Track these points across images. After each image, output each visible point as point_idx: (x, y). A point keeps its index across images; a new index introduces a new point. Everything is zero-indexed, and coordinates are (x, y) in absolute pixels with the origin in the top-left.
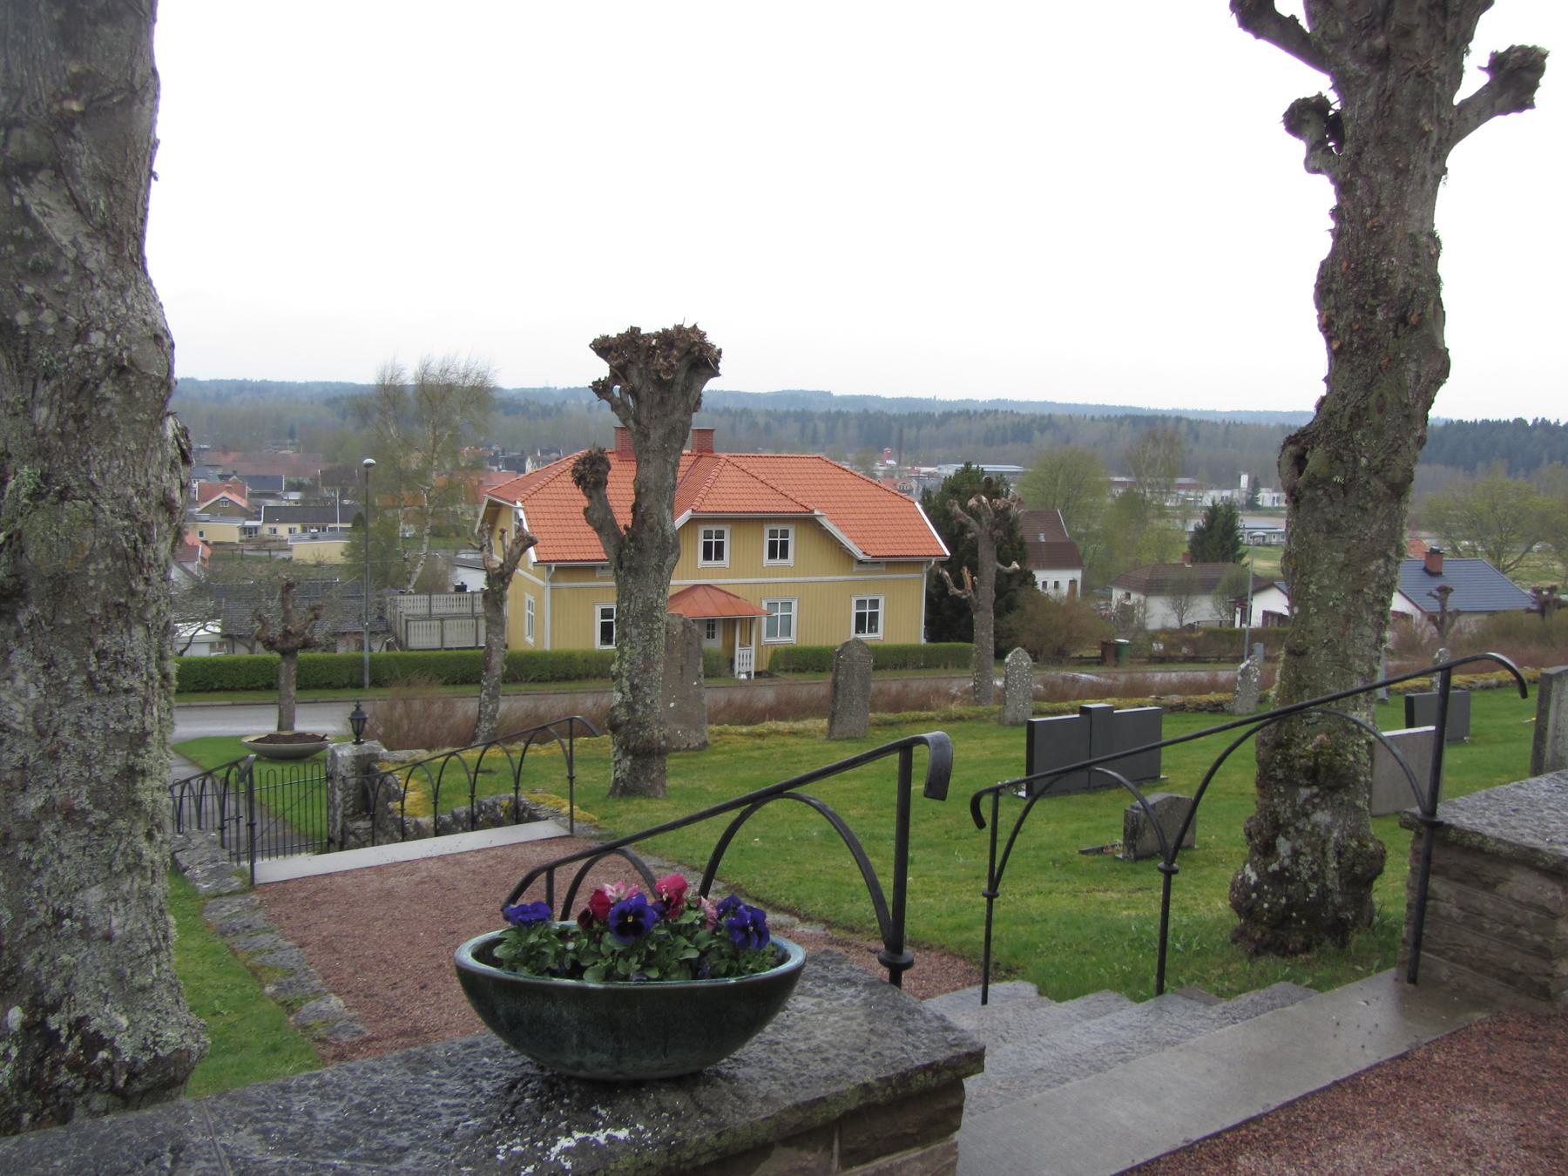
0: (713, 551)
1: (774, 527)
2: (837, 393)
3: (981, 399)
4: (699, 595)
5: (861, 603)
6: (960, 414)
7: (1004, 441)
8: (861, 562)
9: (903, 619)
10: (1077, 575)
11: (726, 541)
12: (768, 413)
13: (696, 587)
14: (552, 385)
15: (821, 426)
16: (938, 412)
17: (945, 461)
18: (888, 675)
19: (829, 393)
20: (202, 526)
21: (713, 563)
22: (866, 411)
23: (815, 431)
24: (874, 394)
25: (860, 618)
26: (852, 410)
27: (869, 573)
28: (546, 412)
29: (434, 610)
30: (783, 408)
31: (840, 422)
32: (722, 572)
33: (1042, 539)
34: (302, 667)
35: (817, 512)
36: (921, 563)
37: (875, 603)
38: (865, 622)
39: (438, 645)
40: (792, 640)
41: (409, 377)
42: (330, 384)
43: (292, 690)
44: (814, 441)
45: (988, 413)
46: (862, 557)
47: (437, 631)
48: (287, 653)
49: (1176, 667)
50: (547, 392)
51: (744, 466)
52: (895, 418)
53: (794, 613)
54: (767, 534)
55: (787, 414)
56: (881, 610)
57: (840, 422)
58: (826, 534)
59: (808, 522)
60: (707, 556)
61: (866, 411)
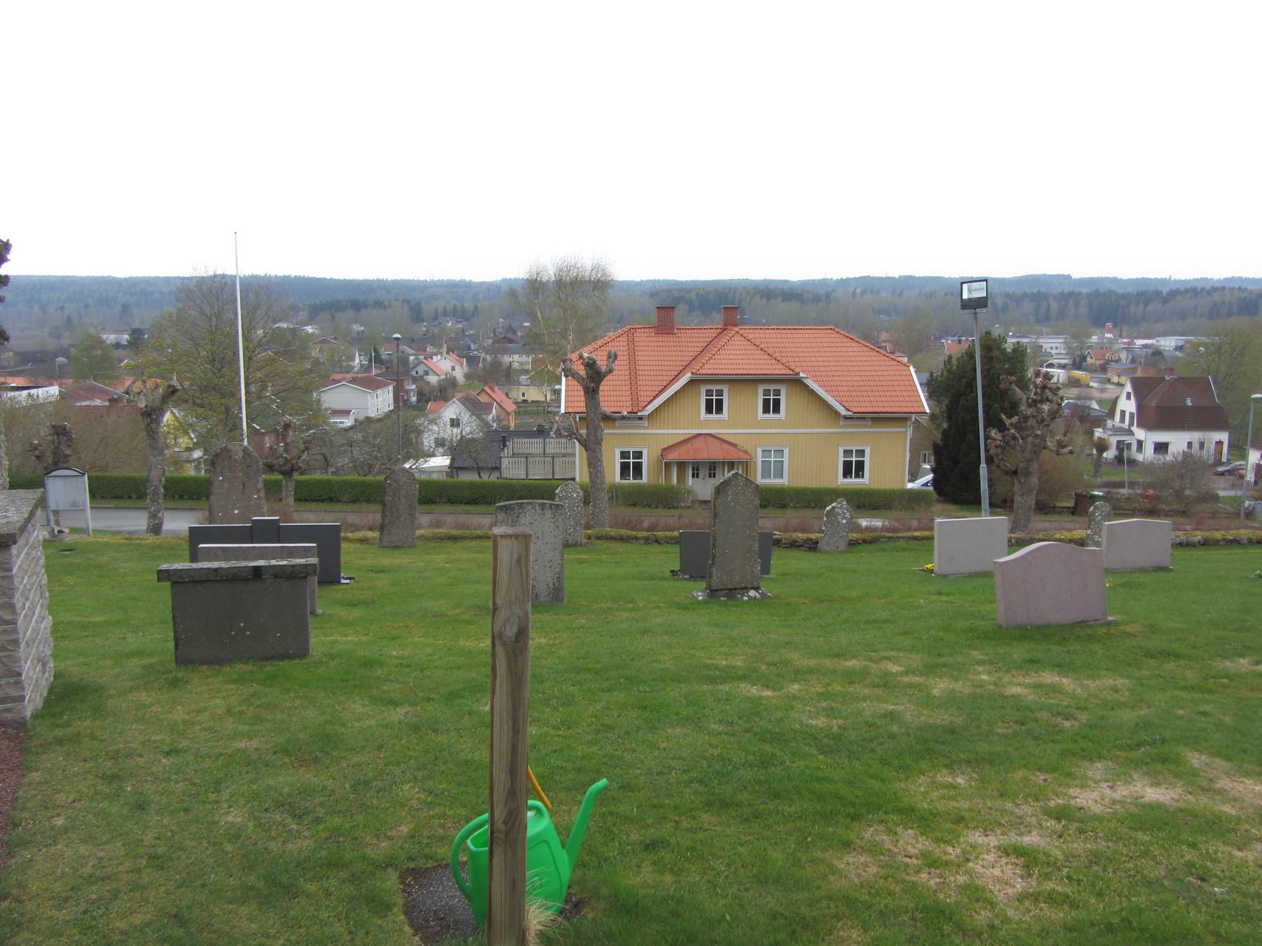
0: (714, 406)
1: (767, 387)
2: (1076, 275)
3: (1216, 277)
4: (698, 443)
5: (847, 453)
6: (1187, 291)
7: (1229, 314)
8: (846, 418)
9: (896, 465)
10: (1224, 437)
11: (783, 398)
12: (1007, 295)
13: (699, 435)
14: (829, 277)
15: (1054, 305)
16: (1165, 291)
17: (1165, 334)
18: (770, 511)
19: (1069, 277)
20: (523, 389)
21: (714, 416)
22: (1097, 291)
23: (1048, 307)
24: (1230, 276)
25: (847, 465)
26: (1085, 290)
27: (857, 427)
28: (816, 299)
29: (547, 451)
30: (1199, 286)
31: (1071, 302)
32: (720, 424)
33: (1189, 402)
34: (299, 485)
35: (802, 375)
36: (906, 419)
37: (861, 453)
38: (853, 468)
39: (523, 476)
40: (784, 481)
41: (550, 274)
42: (659, 281)
43: (291, 500)
44: (1047, 318)
45: (1215, 289)
46: (843, 412)
47: (549, 467)
48: (288, 473)
49: (1056, 517)
50: (823, 282)
51: (750, 337)
52: (1124, 297)
53: (786, 459)
54: (703, 393)
55: (1025, 295)
56: (867, 459)
57: (1071, 302)
58: (812, 392)
59: (795, 382)
60: (766, 410)
61: (1097, 291)
